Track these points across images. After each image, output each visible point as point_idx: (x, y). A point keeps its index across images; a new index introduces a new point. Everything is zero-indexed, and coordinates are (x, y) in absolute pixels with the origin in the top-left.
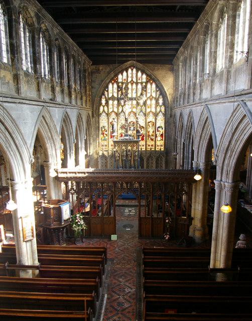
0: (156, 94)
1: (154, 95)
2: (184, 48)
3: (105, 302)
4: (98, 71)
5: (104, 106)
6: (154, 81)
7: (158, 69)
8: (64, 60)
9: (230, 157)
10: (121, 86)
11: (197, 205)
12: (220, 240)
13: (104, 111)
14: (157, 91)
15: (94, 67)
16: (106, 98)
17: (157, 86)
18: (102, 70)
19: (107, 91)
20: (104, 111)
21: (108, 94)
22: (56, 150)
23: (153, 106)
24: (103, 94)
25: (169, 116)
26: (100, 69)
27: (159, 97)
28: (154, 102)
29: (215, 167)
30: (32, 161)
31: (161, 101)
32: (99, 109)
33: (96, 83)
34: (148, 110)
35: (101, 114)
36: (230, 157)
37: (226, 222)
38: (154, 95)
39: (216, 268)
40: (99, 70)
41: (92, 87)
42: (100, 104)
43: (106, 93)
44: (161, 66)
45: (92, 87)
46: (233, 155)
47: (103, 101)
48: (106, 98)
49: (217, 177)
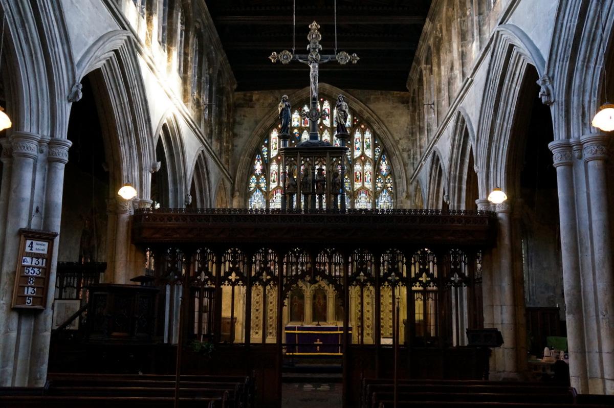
0: (374, 152)
1: (369, 153)
2: (432, 20)
3: (218, 383)
4: (249, 103)
5: (258, 177)
6: (369, 126)
7: (378, 99)
8: (179, 25)
9: (587, 60)
10: (297, 135)
11: (497, 311)
12: (592, 310)
13: (258, 187)
14: (375, 146)
15: (239, 95)
16: (263, 159)
17: (375, 136)
18: (258, 100)
19: (268, 145)
20: (258, 187)
21: (269, 152)
22: (141, 169)
23: (368, 177)
24: (258, 151)
25: (404, 195)
26: (254, 98)
27: (380, 159)
28: (368, 168)
29: (546, 109)
30: (76, 93)
31: (384, 167)
32: (248, 183)
33: (245, 125)
34: (358, 185)
35: (252, 193)
36: (587, 60)
37: (601, 244)
38: (369, 153)
39: (591, 392)
40: (251, 100)
41: (235, 135)
42: (252, 172)
43: (265, 149)
44: (382, 94)
45: (235, 135)
46: (595, 51)
47: (258, 167)
48: (263, 159)
49: (556, 132)
